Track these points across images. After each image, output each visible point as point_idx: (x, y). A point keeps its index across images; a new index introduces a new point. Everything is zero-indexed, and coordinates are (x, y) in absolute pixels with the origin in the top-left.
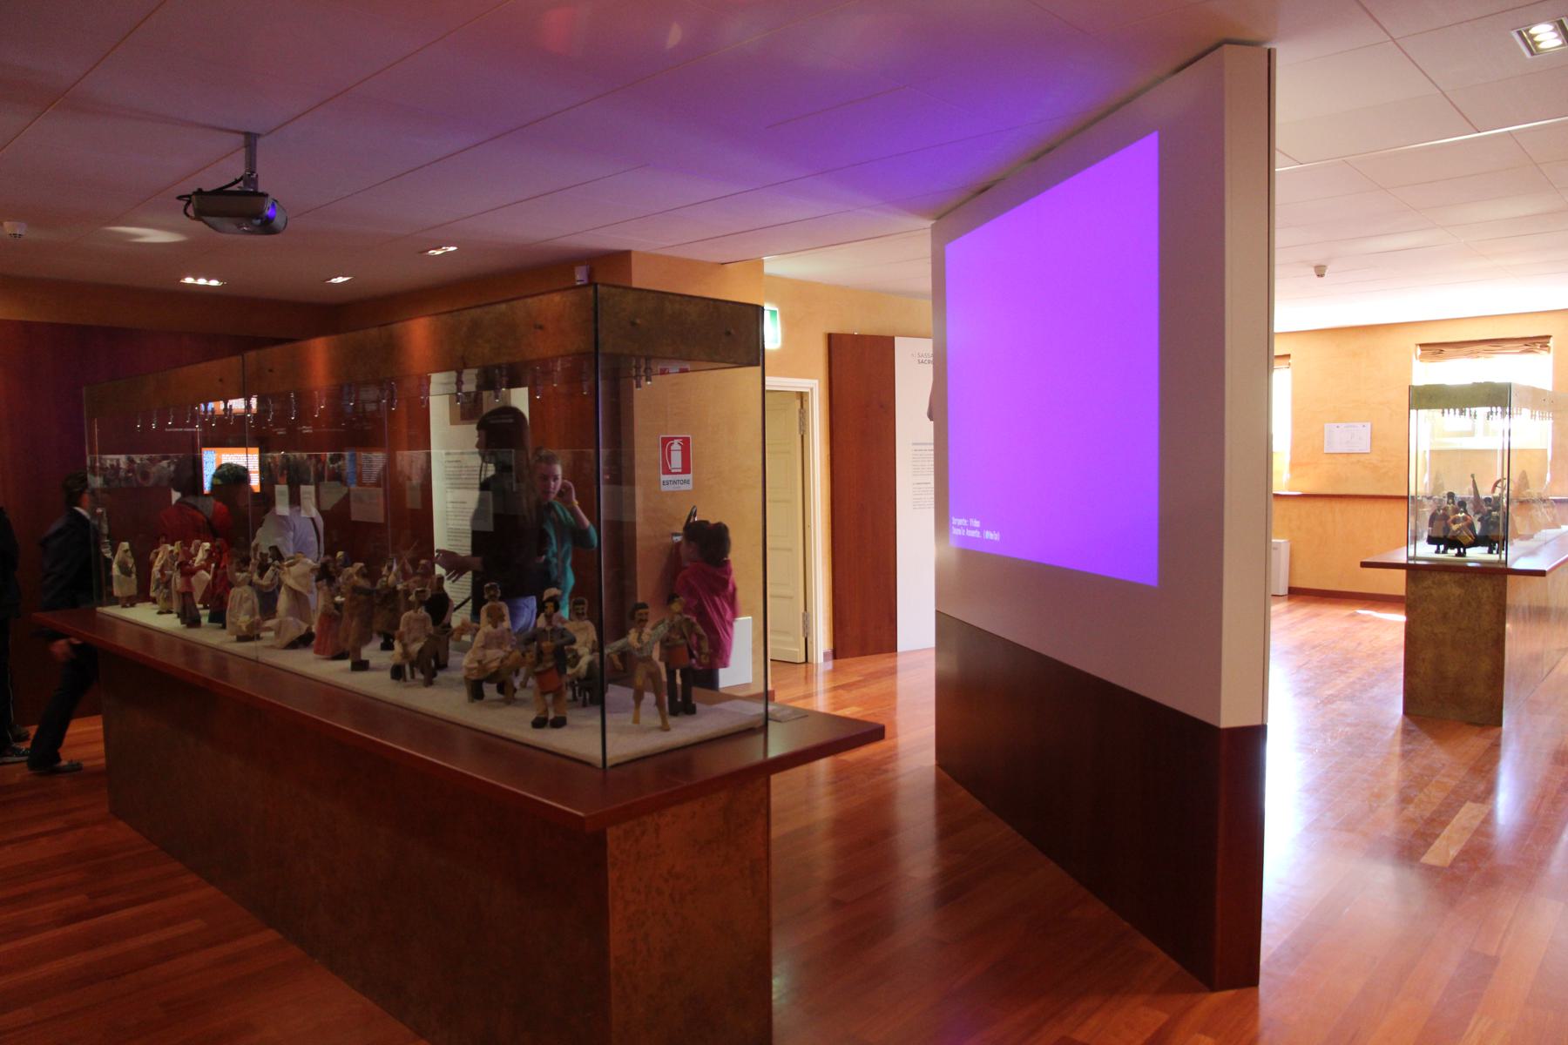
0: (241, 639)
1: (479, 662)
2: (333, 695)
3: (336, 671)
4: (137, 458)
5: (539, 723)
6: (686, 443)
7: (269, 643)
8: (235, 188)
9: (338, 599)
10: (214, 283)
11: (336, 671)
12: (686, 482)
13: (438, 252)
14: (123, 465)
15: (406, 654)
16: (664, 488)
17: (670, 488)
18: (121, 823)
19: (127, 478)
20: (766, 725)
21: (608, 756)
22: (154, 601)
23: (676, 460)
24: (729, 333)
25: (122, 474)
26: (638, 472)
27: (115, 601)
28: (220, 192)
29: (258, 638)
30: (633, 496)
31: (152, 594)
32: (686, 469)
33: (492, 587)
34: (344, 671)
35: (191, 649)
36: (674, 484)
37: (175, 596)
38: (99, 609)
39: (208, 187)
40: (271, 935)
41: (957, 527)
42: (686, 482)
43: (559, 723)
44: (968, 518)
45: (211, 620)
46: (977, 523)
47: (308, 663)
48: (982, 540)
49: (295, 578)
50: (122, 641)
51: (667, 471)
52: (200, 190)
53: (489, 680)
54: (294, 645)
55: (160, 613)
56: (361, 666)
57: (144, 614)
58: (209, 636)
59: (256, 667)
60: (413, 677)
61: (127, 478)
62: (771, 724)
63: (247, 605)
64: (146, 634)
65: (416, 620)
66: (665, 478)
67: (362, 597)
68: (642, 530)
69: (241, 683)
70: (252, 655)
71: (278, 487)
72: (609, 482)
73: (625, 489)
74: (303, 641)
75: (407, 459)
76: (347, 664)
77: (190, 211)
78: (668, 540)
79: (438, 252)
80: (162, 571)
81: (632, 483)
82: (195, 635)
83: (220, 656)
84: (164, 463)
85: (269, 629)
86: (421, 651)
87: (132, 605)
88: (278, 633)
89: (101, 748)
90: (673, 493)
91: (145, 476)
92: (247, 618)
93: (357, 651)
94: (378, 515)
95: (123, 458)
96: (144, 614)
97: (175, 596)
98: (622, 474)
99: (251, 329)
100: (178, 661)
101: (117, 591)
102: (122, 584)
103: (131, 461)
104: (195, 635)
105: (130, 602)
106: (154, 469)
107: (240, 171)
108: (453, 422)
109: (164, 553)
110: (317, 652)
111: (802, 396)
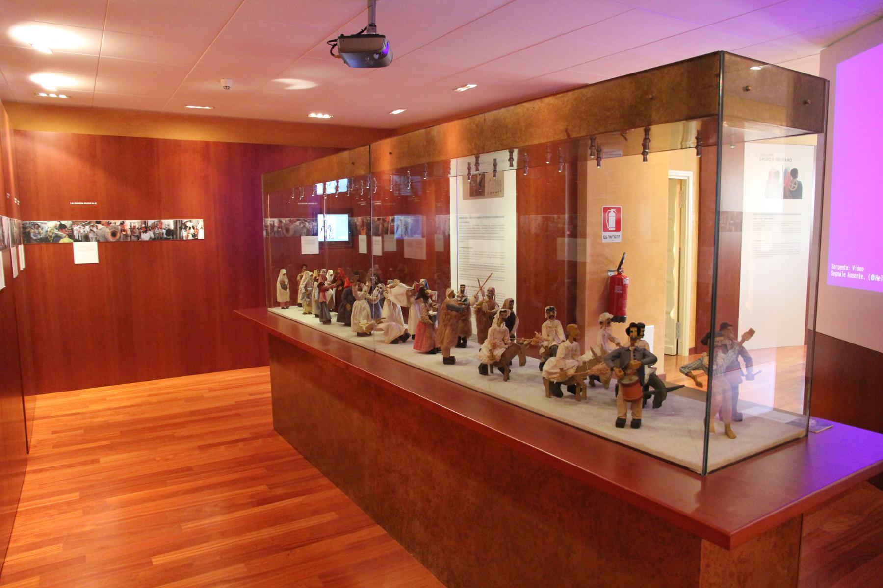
0: (360, 335)
1: (561, 369)
2: (428, 378)
3: (432, 363)
4: (283, 220)
5: (620, 423)
6: (618, 210)
7: (377, 338)
8: (365, 33)
9: (431, 312)
10: (327, 116)
11: (432, 363)
12: (618, 237)
13: (463, 89)
14: (276, 225)
15: (492, 356)
16: (604, 241)
17: (608, 240)
18: (281, 438)
19: (278, 232)
20: (807, 435)
21: (709, 464)
22: (300, 305)
23: (612, 224)
24: (805, 103)
25: (276, 229)
26: (589, 230)
27: (277, 304)
28: (359, 35)
29: (370, 334)
30: (585, 245)
31: (299, 301)
32: (618, 228)
33: (551, 309)
34: (439, 363)
35: (325, 339)
36: (611, 238)
37: (314, 303)
38: (269, 309)
39: (347, 34)
40: (378, 530)
41: (836, 271)
42: (618, 237)
43: (636, 424)
44: (850, 265)
45: (338, 321)
46: (860, 269)
47: (406, 353)
48: (866, 281)
49: (396, 297)
50: (282, 329)
51: (606, 229)
52: (342, 36)
53: (564, 383)
54: (395, 342)
55: (305, 313)
56: (449, 360)
57: (294, 313)
58: (337, 330)
59: (373, 356)
60: (492, 372)
61: (278, 232)
62: (810, 434)
63: (364, 313)
64: (295, 325)
65: (500, 332)
66: (604, 234)
67: (454, 313)
68: (589, 268)
69: (361, 365)
70: (371, 347)
71: (360, 237)
72: (569, 236)
73: (579, 240)
74: (403, 338)
75: (439, 218)
76: (439, 357)
77: (336, 51)
78: (605, 275)
79: (463, 89)
80: (305, 287)
81: (584, 236)
82: (327, 329)
83: (345, 346)
84: (298, 223)
85: (381, 330)
86: (503, 355)
87: (287, 308)
88: (386, 333)
89: (270, 395)
90: (609, 245)
91: (288, 230)
92: (365, 321)
93: (448, 350)
94: (422, 255)
95: (276, 220)
96: (294, 313)
97: (314, 303)
98: (576, 231)
99: (344, 140)
100: (316, 345)
101: (279, 299)
102: (282, 295)
103: (280, 222)
104: (327, 329)
105: (286, 306)
106: (292, 227)
107: (365, 24)
108: (465, 198)
109: (305, 277)
110: (415, 348)
111: (682, 182)
